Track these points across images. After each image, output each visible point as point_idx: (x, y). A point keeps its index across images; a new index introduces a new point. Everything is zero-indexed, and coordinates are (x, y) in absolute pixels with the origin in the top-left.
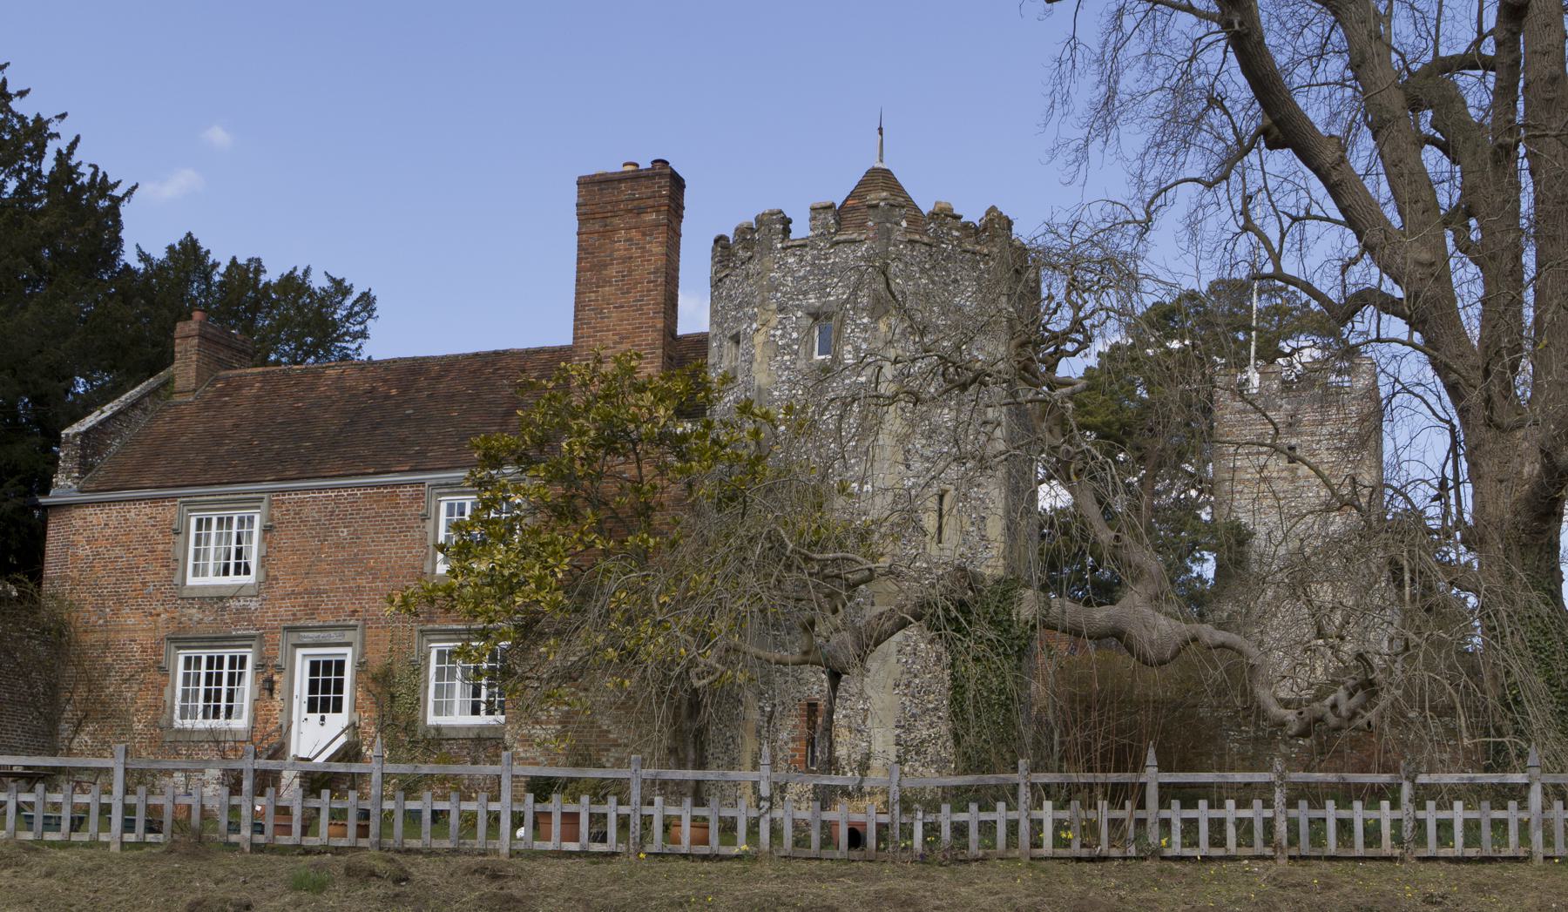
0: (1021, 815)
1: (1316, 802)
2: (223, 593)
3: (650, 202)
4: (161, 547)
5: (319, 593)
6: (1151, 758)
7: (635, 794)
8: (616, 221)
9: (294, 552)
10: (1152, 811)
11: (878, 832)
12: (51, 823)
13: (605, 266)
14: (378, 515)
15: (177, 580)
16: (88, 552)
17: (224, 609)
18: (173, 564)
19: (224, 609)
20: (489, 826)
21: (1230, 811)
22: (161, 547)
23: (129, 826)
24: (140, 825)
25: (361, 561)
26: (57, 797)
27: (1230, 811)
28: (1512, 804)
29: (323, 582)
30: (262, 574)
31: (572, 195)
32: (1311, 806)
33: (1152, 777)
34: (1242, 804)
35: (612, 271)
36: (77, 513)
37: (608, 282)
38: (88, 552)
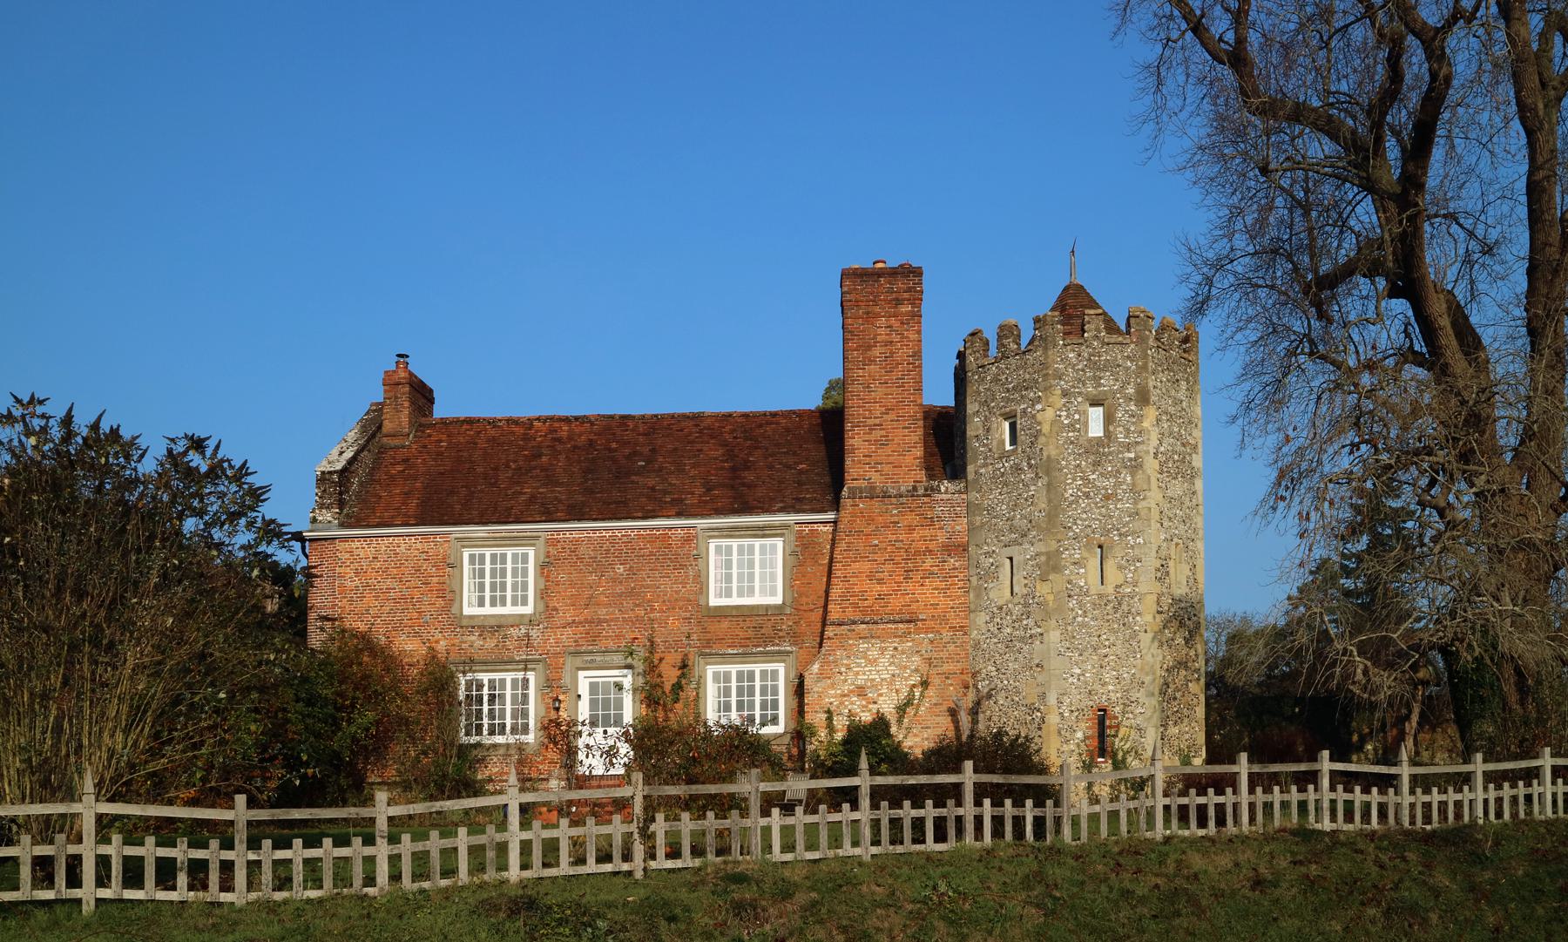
0: (382, 850)
1: (448, 829)
2: (503, 622)
3: (906, 295)
4: (435, 580)
5: (600, 622)
6: (864, 764)
7: (241, 837)
8: (877, 309)
9: (572, 585)
10: (515, 835)
11: (924, 834)
12: (133, 876)
13: (869, 348)
14: (651, 554)
15: (454, 610)
16: (357, 583)
17: (505, 637)
18: (449, 595)
19: (505, 637)
20: (1224, 815)
21: (463, 839)
22: (435, 580)
23: (102, 881)
24: (800, 845)
25: (638, 594)
26: (727, 823)
27: (463, 839)
28: (617, 818)
29: (602, 612)
30: (541, 607)
31: (1013, 321)
32: (443, 835)
33: (88, 809)
34: (939, 804)
35: (877, 351)
36: (340, 545)
37: (872, 361)
38: (357, 583)
